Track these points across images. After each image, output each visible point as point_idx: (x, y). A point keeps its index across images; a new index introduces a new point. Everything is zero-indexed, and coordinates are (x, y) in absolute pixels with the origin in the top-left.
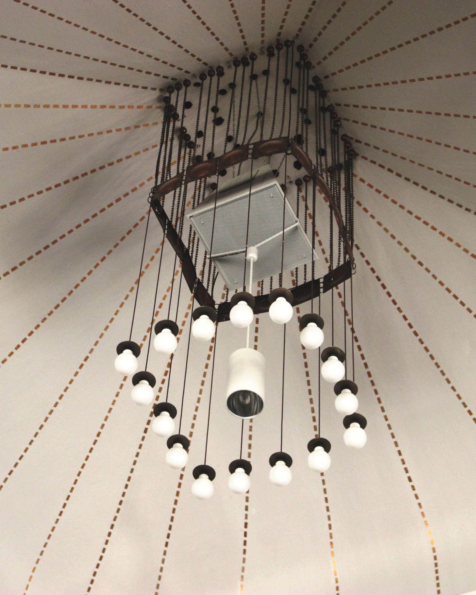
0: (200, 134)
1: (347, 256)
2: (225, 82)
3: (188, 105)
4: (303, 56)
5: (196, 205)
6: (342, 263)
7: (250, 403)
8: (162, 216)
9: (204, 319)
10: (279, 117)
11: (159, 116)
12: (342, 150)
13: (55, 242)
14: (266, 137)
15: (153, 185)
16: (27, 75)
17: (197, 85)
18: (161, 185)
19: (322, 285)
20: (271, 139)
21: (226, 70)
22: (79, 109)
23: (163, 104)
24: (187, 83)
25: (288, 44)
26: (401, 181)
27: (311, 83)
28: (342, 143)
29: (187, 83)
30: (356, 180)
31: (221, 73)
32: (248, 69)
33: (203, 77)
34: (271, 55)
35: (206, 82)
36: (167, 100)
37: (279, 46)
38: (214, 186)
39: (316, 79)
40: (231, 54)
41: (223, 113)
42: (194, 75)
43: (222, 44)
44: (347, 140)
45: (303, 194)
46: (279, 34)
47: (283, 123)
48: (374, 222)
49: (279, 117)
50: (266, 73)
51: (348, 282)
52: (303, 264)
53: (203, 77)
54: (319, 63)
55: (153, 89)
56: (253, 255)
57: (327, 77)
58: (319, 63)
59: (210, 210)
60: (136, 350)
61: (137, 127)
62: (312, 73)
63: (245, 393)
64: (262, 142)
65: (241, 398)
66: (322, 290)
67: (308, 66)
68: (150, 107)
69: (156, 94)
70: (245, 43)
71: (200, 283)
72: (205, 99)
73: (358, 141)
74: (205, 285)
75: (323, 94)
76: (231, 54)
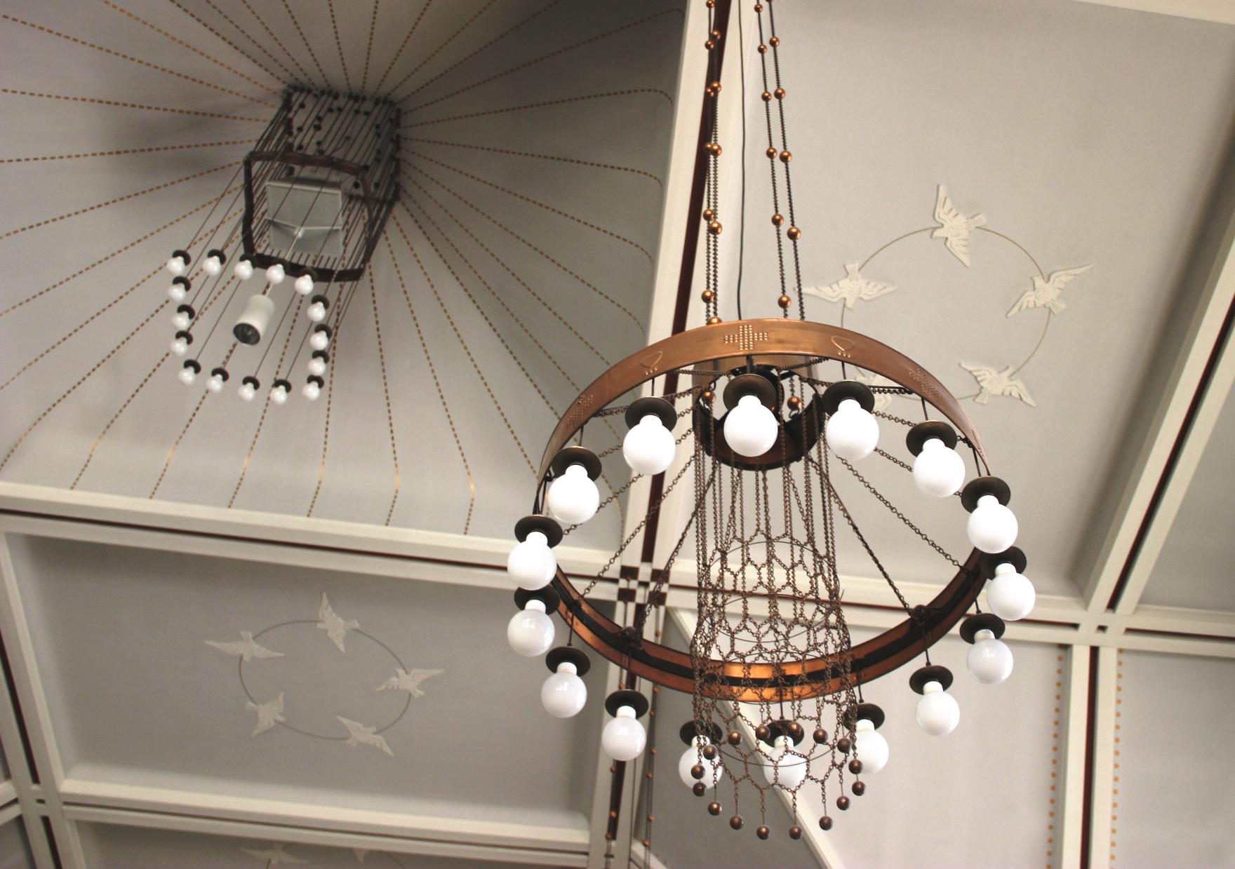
0: (300, 129)
1: (362, 266)
2: (337, 104)
3: (302, 106)
4: (398, 117)
5: (277, 177)
6: (356, 267)
7: (251, 335)
8: (248, 173)
9: (248, 263)
10: (364, 148)
11: (279, 103)
12: (391, 193)
13: (158, 149)
14: (349, 158)
15: (252, 149)
16: (206, 30)
17: (316, 96)
18: (258, 152)
19: (335, 276)
20: (351, 162)
21: (341, 98)
22: (419, 258)
23: (285, 96)
24: (309, 91)
25: (392, 103)
26: (420, 232)
27: (394, 138)
28: (393, 188)
29: (309, 91)
30: (391, 216)
31: (336, 96)
32: (357, 105)
33: (323, 93)
34: (377, 103)
35: (324, 98)
36: (290, 95)
37: (385, 102)
38: (291, 171)
39: (398, 136)
40: (350, 89)
41: (326, 125)
42: (317, 89)
43: (347, 79)
44: (398, 187)
45: (351, 206)
46: (389, 94)
47: (334, 124)
48: (388, 250)
49: (364, 148)
50: (367, 114)
51: (355, 283)
52: (335, 256)
53: (323, 93)
54: (405, 127)
55: (284, 82)
56: (300, 233)
57: (406, 139)
58: (405, 127)
59: (286, 188)
60: (187, 260)
61: (259, 101)
62: (399, 131)
63: (250, 327)
64: (343, 160)
65: (245, 330)
66: (333, 279)
67: (398, 125)
68: (275, 93)
69: (284, 87)
70: (363, 87)
71: (251, 232)
72: (317, 109)
73: (405, 191)
74: (254, 234)
75: (398, 148)
76: (350, 89)
